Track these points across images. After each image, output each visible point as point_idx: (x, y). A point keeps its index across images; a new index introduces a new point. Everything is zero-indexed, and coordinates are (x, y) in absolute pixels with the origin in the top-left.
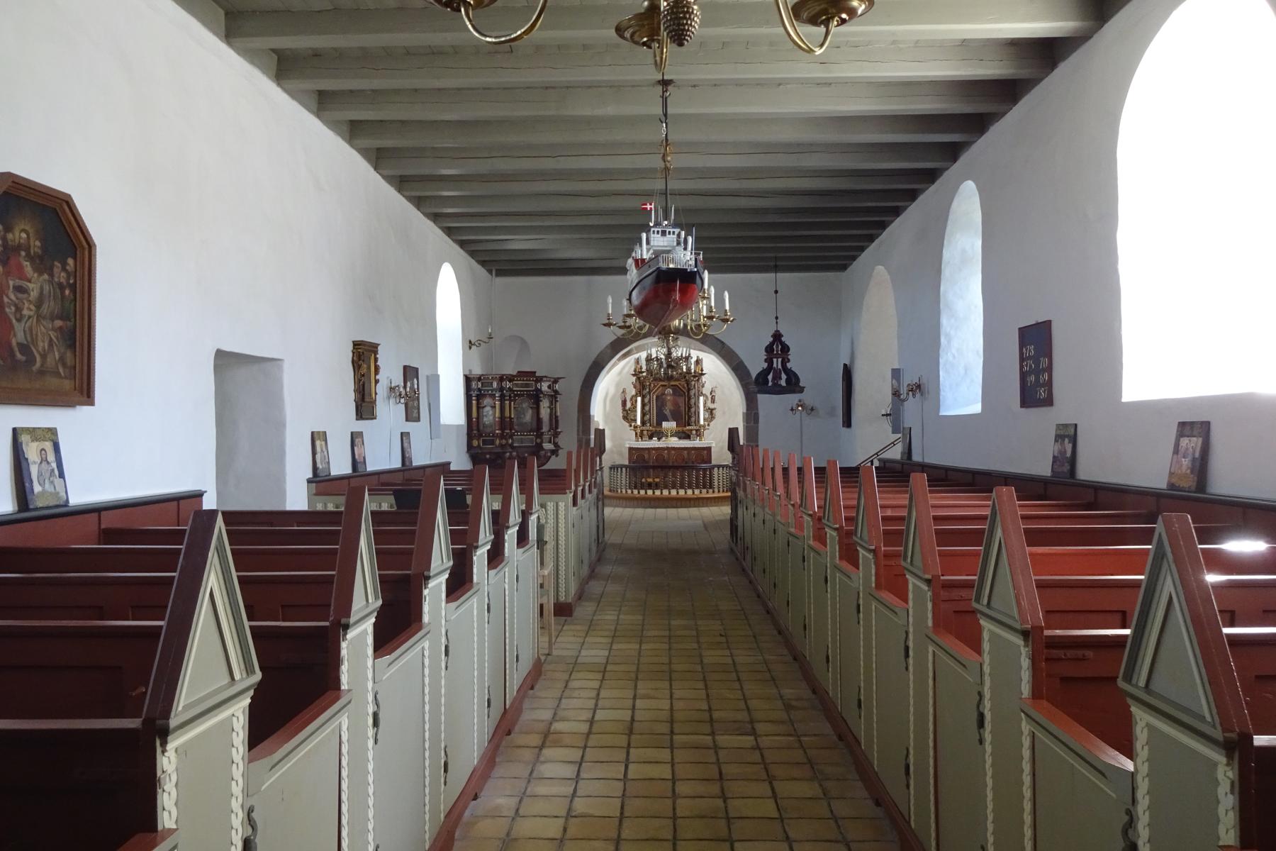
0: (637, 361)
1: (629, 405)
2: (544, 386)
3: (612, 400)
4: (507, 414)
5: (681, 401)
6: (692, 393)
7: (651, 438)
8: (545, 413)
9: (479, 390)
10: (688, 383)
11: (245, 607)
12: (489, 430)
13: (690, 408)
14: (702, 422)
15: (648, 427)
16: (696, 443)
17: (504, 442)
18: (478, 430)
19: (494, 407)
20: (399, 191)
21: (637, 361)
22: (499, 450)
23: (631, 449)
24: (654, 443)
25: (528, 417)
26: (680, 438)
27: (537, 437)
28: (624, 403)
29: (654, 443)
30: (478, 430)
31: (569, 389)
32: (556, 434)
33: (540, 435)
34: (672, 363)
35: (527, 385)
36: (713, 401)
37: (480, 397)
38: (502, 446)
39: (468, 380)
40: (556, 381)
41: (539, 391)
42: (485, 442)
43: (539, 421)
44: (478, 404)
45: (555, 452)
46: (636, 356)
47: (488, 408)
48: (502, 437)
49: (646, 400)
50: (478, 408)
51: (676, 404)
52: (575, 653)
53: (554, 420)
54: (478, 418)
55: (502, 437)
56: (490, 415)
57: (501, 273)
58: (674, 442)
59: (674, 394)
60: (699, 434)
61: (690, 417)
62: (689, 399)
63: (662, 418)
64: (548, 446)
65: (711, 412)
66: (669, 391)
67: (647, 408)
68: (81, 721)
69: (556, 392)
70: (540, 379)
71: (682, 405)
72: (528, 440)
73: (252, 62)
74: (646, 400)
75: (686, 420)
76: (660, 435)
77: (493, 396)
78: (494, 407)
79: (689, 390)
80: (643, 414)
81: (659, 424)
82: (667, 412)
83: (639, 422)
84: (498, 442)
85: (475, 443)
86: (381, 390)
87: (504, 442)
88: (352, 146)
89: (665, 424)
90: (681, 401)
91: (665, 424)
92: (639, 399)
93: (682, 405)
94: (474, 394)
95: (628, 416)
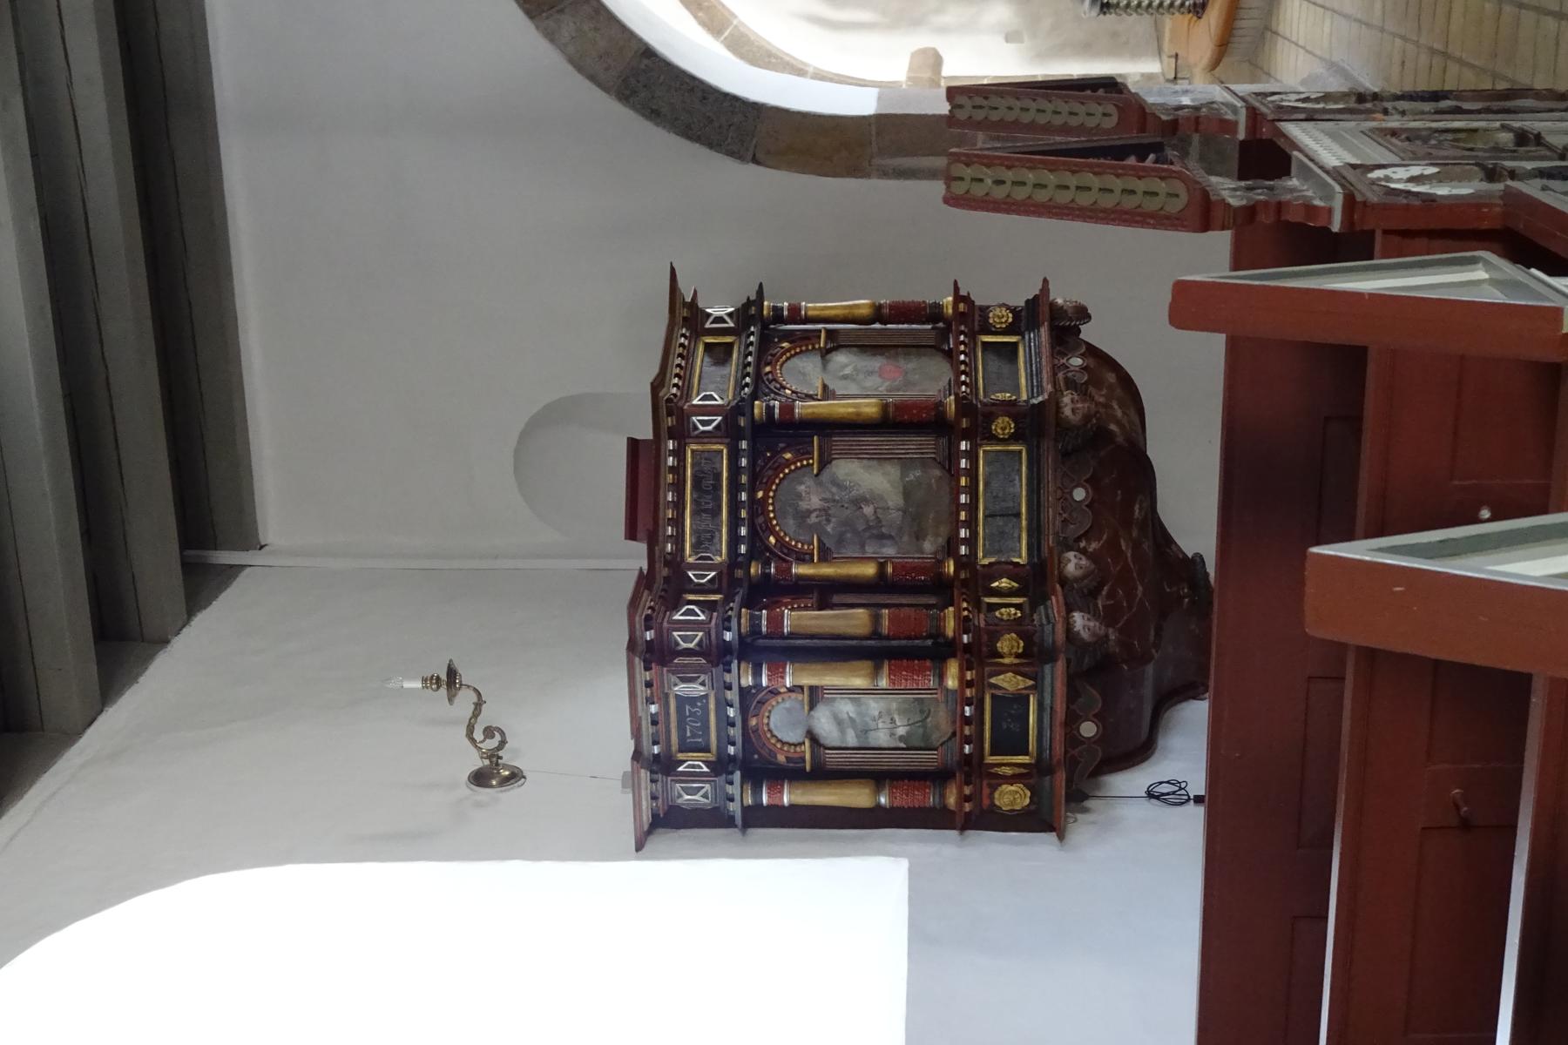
2: (714, 389)
4: (853, 620)
8: (851, 385)
9: (721, 766)
11: (1326, 918)
12: (941, 721)
17: (1008, 644)
18: (940, 777)
19: (815, 696)
20: (164, 642)
22: (1056, 674)
25: (871, 479)
27: (980, 430)
30: (940, 777)
31: (737, 235)
32: (971, 316)
33: (975, 420)
35: (706, 485)
37: (760, 766)
38: (1035, 656)
39: (665, 823)
40: (686, 316)
41: (733, 422)
42: (1010, 741)
43: (896, 421)
44: (795, 774)
45: (1065, 326)
47: (824, 723)
48: (979, 655)
50: (822, 774)
53: (896, 328)
54: (878, 777)
55: (979, 655)
56: (858, 710)
57: (209, 525)
64: (1025, 382)
69: (748, 314)
70: (671, 413)
72: (1002, 475)
73: (133, 679)
77: (750, 700)
78: (815, 696)
84: (1009, 682)
85: (1012, 797)
87: (1008, 644)
88: (71, 735)
94: (739, 795)
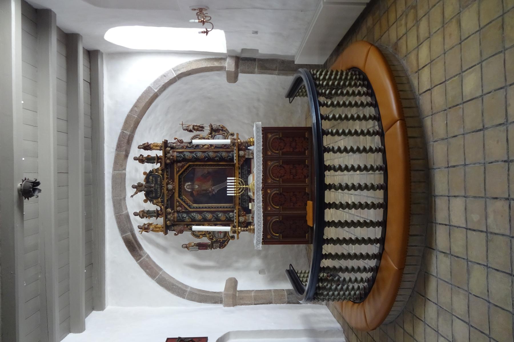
0: (145, 228)
1: (205, 240)
3: (201, 258)
5: (200, 171)
6: (188, 155)
7: (249, 211)
10: (174, 161)
13: (210, 159)
14: (228, 141)
15: (234, 215)
16: (256, 151)
21: (145, 228)
23: (265, 241)
24: (257, 207)
26: (250, 172)
28: (202, 246)
29: (257, 207)
34: (150, 188)
36: (201, 128)
46: (137, 231)
49: (198, 217)
51: (205, 178)
52: (428, 321)
58: (255, 180)
59: (191, 180)
60: (244, 146)
61: (222, 159)
62: (197, 159)
63: (222, 196)
65: (214, 132)
66: (187, 186)
67: (209, 216)
68: (112, 213)
71: (207, 170)
74: (198, 217)
75: (228, 162)
76: (245, 199)
79: (185, 160)
80: (216, 222)
81: (231, 199)
82: (216, 189)
83: (228, 229)
86: (216, 154)
89: (231, 193)
90: (200, 171)
91: (231, 193)
92: (195, 228)
93: (207, 170)
95: (219, 242)
